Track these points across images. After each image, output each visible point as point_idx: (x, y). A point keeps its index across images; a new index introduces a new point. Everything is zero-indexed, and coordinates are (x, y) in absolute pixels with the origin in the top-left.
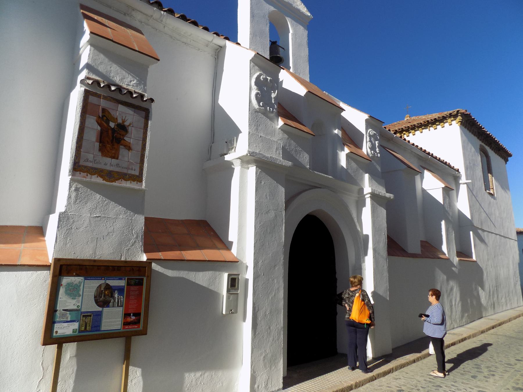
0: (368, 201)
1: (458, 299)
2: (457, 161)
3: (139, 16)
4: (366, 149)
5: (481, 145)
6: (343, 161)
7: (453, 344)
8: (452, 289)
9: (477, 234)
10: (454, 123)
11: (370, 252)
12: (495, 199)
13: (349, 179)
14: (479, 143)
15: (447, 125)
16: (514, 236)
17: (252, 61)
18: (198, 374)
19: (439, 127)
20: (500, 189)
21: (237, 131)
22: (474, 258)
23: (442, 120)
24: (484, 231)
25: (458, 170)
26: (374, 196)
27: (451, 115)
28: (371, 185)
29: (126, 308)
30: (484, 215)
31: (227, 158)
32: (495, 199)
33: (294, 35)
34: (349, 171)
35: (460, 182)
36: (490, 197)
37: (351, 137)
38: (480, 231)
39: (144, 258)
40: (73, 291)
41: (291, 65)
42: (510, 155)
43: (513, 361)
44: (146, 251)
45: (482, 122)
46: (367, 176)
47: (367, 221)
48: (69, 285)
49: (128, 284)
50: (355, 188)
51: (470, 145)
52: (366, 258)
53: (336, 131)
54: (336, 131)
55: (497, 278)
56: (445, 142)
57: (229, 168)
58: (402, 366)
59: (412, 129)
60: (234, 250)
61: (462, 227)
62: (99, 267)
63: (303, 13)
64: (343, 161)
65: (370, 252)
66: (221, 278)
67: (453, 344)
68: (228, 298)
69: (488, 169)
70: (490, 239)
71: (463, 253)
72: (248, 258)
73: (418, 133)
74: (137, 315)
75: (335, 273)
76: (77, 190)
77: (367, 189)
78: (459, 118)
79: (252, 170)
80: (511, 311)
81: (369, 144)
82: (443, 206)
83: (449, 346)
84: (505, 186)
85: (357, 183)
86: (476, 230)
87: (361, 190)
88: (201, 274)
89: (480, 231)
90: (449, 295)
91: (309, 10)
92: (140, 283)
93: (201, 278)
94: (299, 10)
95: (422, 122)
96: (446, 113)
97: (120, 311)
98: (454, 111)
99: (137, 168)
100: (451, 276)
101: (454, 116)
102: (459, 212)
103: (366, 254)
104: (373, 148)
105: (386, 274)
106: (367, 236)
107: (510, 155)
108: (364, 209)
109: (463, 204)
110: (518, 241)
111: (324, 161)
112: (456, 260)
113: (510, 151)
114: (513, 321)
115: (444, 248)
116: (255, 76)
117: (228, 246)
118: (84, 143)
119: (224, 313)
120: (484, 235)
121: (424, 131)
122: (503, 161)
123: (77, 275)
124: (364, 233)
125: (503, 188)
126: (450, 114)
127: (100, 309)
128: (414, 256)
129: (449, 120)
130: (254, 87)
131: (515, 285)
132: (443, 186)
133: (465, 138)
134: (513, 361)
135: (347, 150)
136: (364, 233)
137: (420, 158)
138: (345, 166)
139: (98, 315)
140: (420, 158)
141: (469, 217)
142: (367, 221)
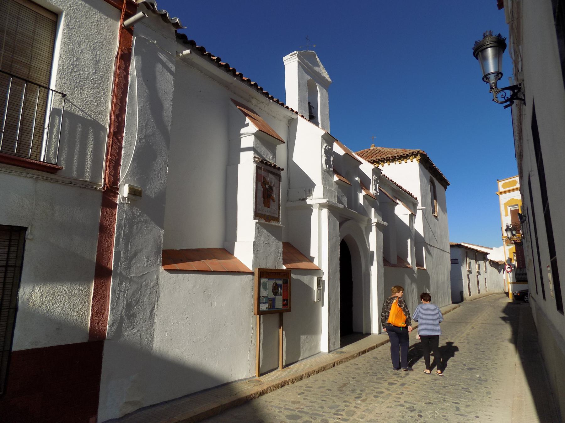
0: (374, 228)
1: (416, 297)
2: (416, 192)
3: (254, 101)
4: (372, 190)
5: (430, 177)
6: (361, 201)
7: (383, 343)
8: (413, 290)
9: (427, 250)
10: (414, 160)
11: (375, 263)
12: (437, 220)
13: (364, 212)
14: (429, 175)
15: (409, 161)
16: (448, 249)
17: (323, 137)
18: (306, 336)
19: (403, 162)
20: (441, 213)
21: (313, 185)
22: (425, 267)
23: (405, 157)
24: (431, 246)
25: (416, 199)
26: (378, 225)
27: (413, 154)
28: (375, 217)
29: (283, 297)
30: (431, 233)
31: (309, 202)
32: (437, 220)
33: (321, 97)
34: (365, 207)
35: (418, 208)
36: (433, 217)
37: (364, 183)
38: (429, 246)
39: (284, 268)
40: (265, 288)
41: (320, 121)
42: (449, 184)
43: (455, 332)
44: (285, 263)
45: (433, 160)
46: (373, 210)
47: (373, 241)
48: (263, 282)
49: (283, 283)
50: (366, 219)
51: (424, 178)
52: (372, 267)
53: (357, 179)
54: (357, 179)
55: (438, 282)
56: (407, 175)
57: (309, 209)
58: (553, 252)
59: (382, 161)
60: (316, 262)
61: (419, 242)
62: (275, 273)
63: (327, 80)
64: (361, 201)
65: (375, 263)
66: (313, 280)
67: (383, 343)
68: (317, 292)
69: (434, 196)
70: (434, 252)
71: (419, 263)
72: (325, 268)
73: (386, 165)
74: (287, 300)
75: (351, 277)
76: (258, 228)
77: (374, 219)
78: (419, 157)
79: (325, 212)
80: (445, 307)
81: (374, 187)
82: (409, 228)
83: (387, 341)
84: (444, 209)
85: (366, 214)
86: (426, 245)
87: (370, 220)
88: (306, 277)
89: (429, 246)
90: (412, 294)
91: (330, 77)
92: (287, 283)
93: (305, 279)
94: (324, 78)
95: (390, 156)
96: (408, 151)
97: (281, 297)
98: (416, 151)
99: (277, 212)
100: (413, 280)
101: (415, 155)
102: (416, 231)
103: (372, 264)
104: (376, 190)
105: (383, 278)
106: (373, 252)
107: (449, 184)
108: (371, 233)
109: (419, 226)
110: (451, 254)
111: (353, 200)
112: (416, 268)
113: (449, 180)
114: (448, 314)
115: (409, 260)
116: (324, 147)
117: (311, 260)
118: (258, 200)
119: (315, 300)
120: (431, 249)
121: (391, 163)
122: (443, 188)
123: (266, 278)
124: (371, 250)
125: (443, 210)
126: (413, 153)
127: (274, 297)
128: (394, 266)
129: (411, 158)
130: (324, 155)
131: (448, 287)
132: (410, 213)
133: (421, 172)
134: (455, 332)
135: (364, 193)
136: (371, 250)
137: (393, 190)
138: (362, 204)
139: (274, 300)
140: (393, 190)
141: (423, 235)
142: (373, 241)
